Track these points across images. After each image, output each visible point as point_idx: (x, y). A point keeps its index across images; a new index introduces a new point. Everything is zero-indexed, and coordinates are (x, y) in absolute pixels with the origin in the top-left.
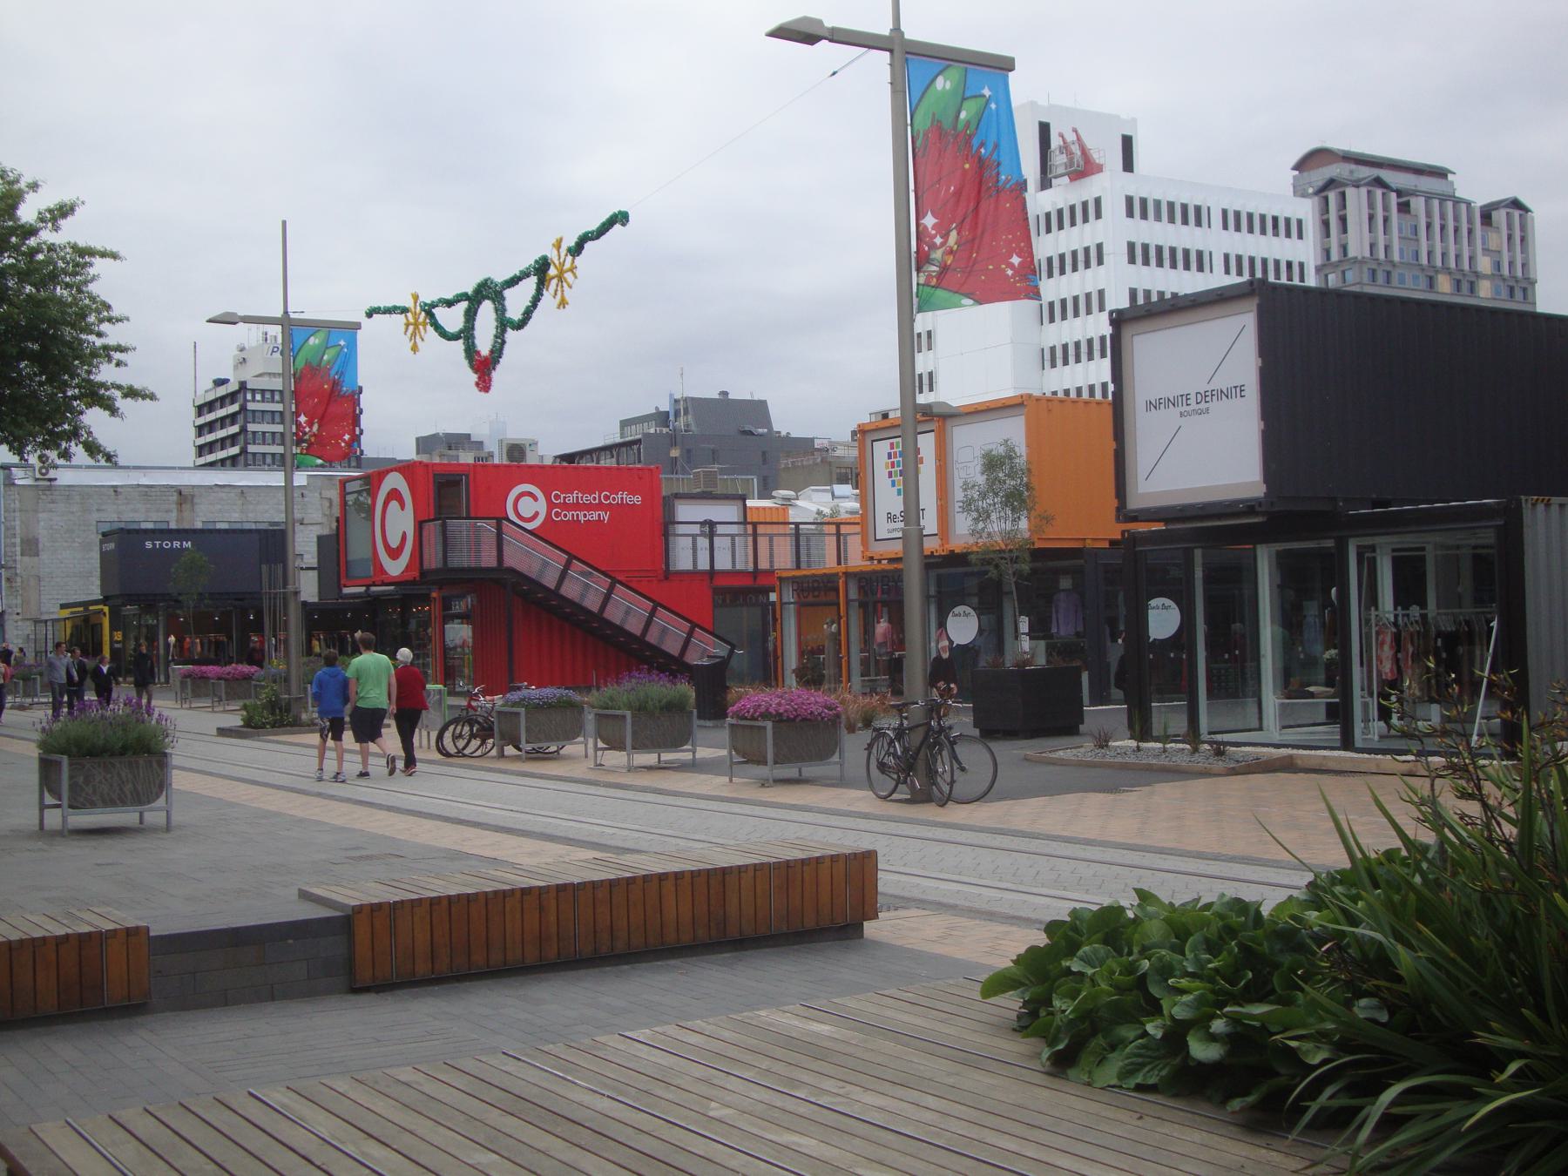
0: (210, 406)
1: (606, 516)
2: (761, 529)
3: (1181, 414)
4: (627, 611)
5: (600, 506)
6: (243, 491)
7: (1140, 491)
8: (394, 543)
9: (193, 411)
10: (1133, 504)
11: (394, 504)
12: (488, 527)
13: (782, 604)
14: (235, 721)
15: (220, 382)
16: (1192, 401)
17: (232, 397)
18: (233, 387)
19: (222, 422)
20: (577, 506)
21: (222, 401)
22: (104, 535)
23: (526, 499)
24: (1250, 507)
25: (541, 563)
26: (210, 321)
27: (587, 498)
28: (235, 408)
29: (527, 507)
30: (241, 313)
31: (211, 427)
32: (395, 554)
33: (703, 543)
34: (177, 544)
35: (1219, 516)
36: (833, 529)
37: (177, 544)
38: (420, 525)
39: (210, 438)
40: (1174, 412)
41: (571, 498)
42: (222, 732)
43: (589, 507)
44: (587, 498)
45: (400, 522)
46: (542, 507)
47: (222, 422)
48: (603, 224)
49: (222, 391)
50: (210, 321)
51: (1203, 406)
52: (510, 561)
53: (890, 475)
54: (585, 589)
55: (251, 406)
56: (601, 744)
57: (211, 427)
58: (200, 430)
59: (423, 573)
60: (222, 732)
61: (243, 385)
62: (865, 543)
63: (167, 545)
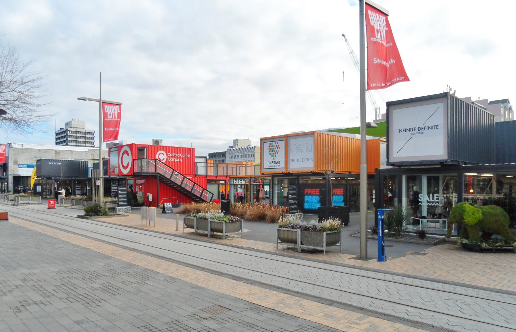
0: (59, 134)
1: (181, 160)
2: (238, 166)
3: (412, 134)
4: (188, 185)
5: (180, 157)
6: (72, 152)
7: (394, 156)
8: (125, 165)
9: (55, 135)
10: (391, 160)
11: (125, 155)
12: (153, 162)
13: (250, 184)
14: (83, 213)
15: (61, 129)
16: (417, 130)
17: (64, 132)
18: (64, 130)
19: (62, 137)
20: (175, 157)
21: (62, 133)
22: (38, 160)
23: (162, 155)
24: (442, 163)
25: (167, 172)
26: (78, 99)
27: (177, 155)
28: (65, 134)
29: (162, 157)
30: (88, 97)
31: (59, 138)
32: (125, 168)
33: (234, 169)
34: (58, 164)
35: (430, 165)
36: (235, 166)
37: (58, 164)
38: (133, 161)
39: (59, 141)
40: (409, 133)
41: (173, 155)
42: (79, 217)
43: (177, 157)
44: (177, 155)
45: (127, 160)
46: (165, 157)
47: (62, 137)
48: (360, 11)
49: (62, 131)
50: (78, 99)
51: (421, 131)
52: (158, 171)
53: (269, 151)
54: (177, 179)
55: (69, 134)
56: (185, 227)
57: (59, 138)
58: (57, 139)
59: (134, 173)
60: (79, 217)
61: (67, 130)
62: (261, 169)
63: (55, 164)
